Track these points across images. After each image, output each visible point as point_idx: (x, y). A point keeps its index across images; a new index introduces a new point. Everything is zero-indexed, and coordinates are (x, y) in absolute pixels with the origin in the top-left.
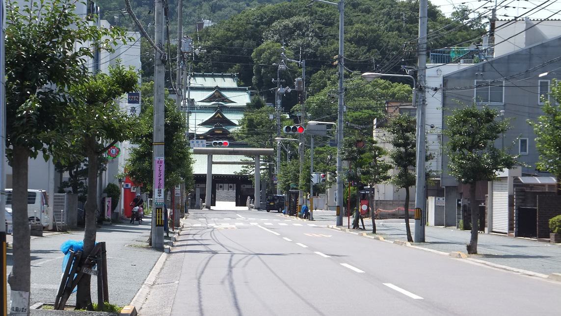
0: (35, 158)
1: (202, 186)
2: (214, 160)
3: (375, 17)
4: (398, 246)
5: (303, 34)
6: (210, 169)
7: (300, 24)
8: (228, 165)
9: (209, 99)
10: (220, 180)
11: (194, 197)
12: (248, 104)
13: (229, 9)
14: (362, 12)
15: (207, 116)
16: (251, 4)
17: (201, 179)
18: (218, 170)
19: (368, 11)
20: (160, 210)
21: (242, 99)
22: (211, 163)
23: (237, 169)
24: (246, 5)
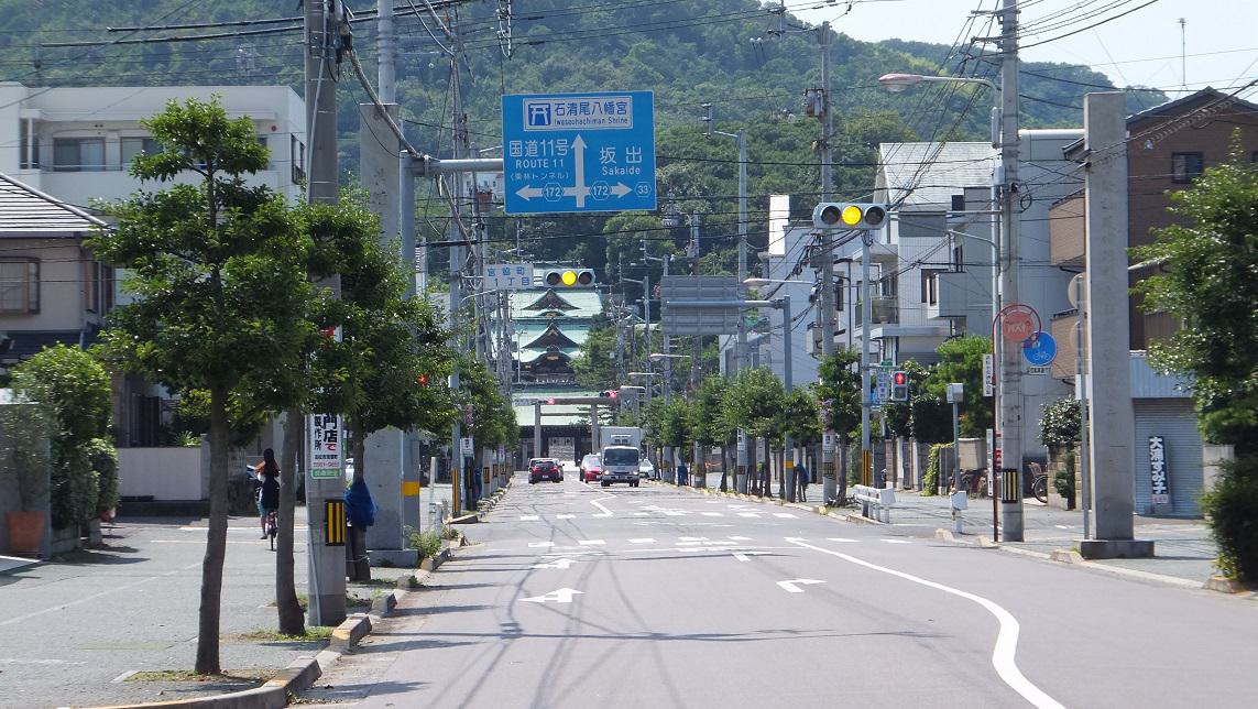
0: (1091, 552)
1: (529, 441)
2: (542, 412)
3: (801, 158)
4: (853, 524)
5: (684, 193)
6: (538, 420)
7: (679, 176)
8: (560, 413)
9: (539, 305)
10: (551, 433)
11: (520, 456)
12: (595, 316)
13: (577, 76)
14: (781, 150)
15: (535, 335)
16: (623, 61)
17: (527, 432)
18: (545, 421)
19: (791, 147)
20: (331, 540)
21: (588, 304)
22: (539, 415)
23: (575, 420)
24: (612, 66)
